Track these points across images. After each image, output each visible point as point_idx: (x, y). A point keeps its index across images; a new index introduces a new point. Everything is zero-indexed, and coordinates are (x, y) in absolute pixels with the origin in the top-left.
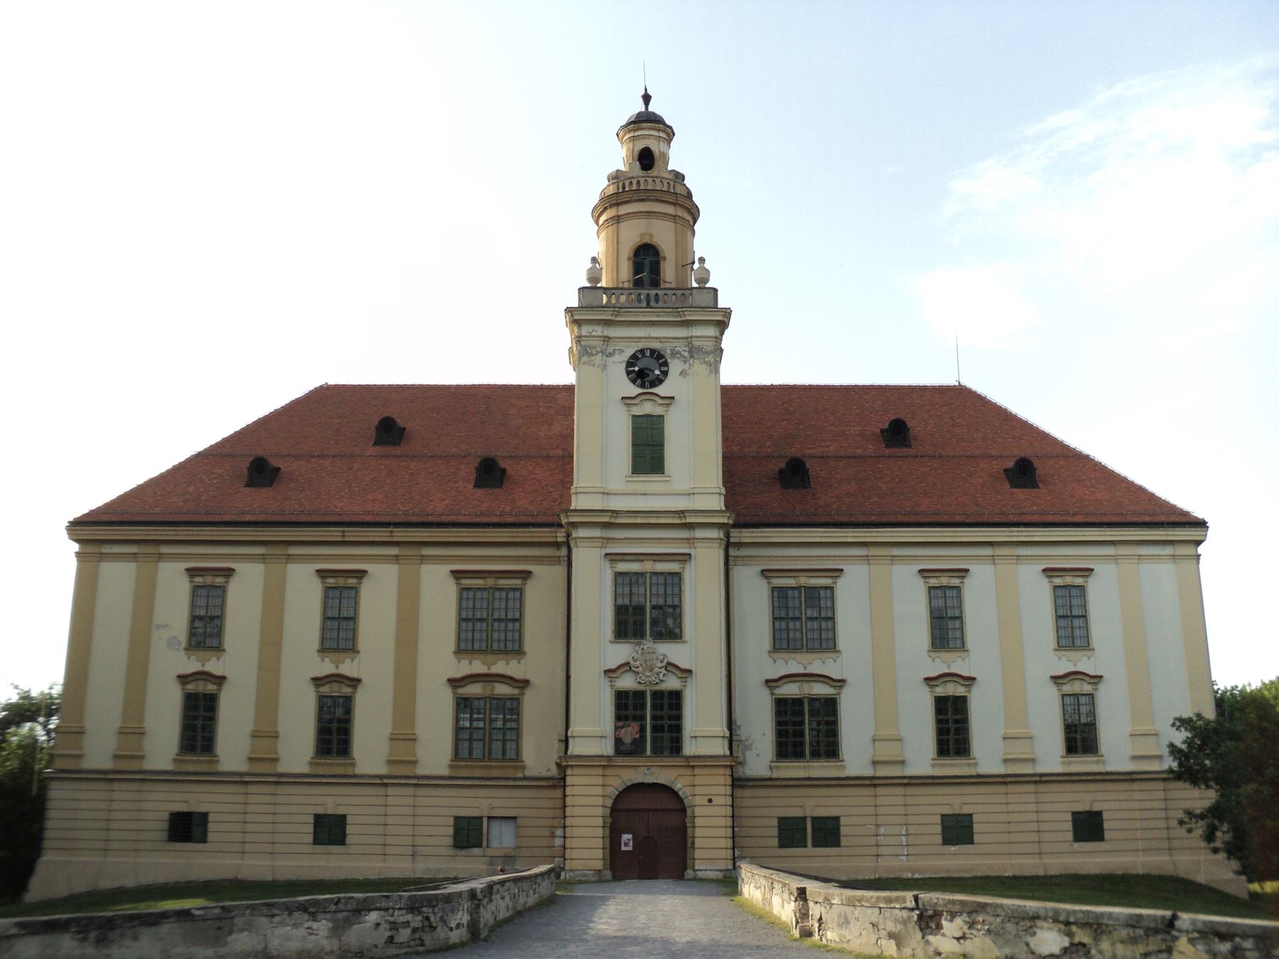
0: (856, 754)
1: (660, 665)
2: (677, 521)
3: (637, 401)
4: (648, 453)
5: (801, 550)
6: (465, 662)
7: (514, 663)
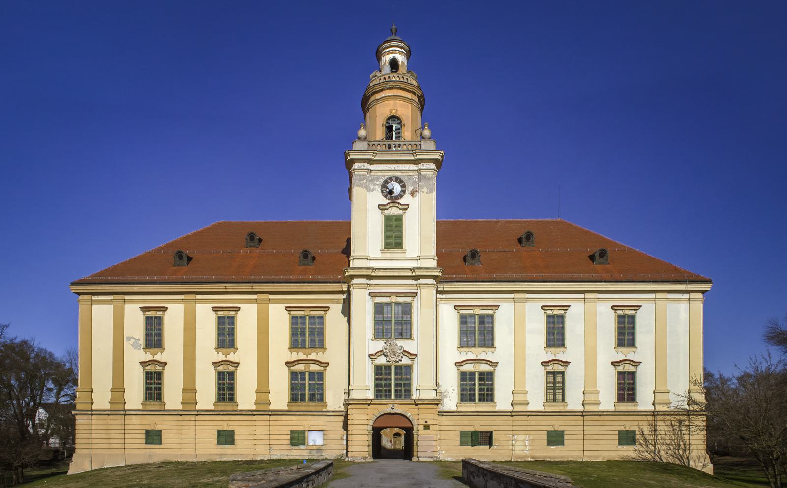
0: (502, 401)
1: (399, 352)
2: (410, 274)
3: (387, 207)
4: (394, 236)
5: (477, 295)
6: (294, 354)
7: (320, 354)
